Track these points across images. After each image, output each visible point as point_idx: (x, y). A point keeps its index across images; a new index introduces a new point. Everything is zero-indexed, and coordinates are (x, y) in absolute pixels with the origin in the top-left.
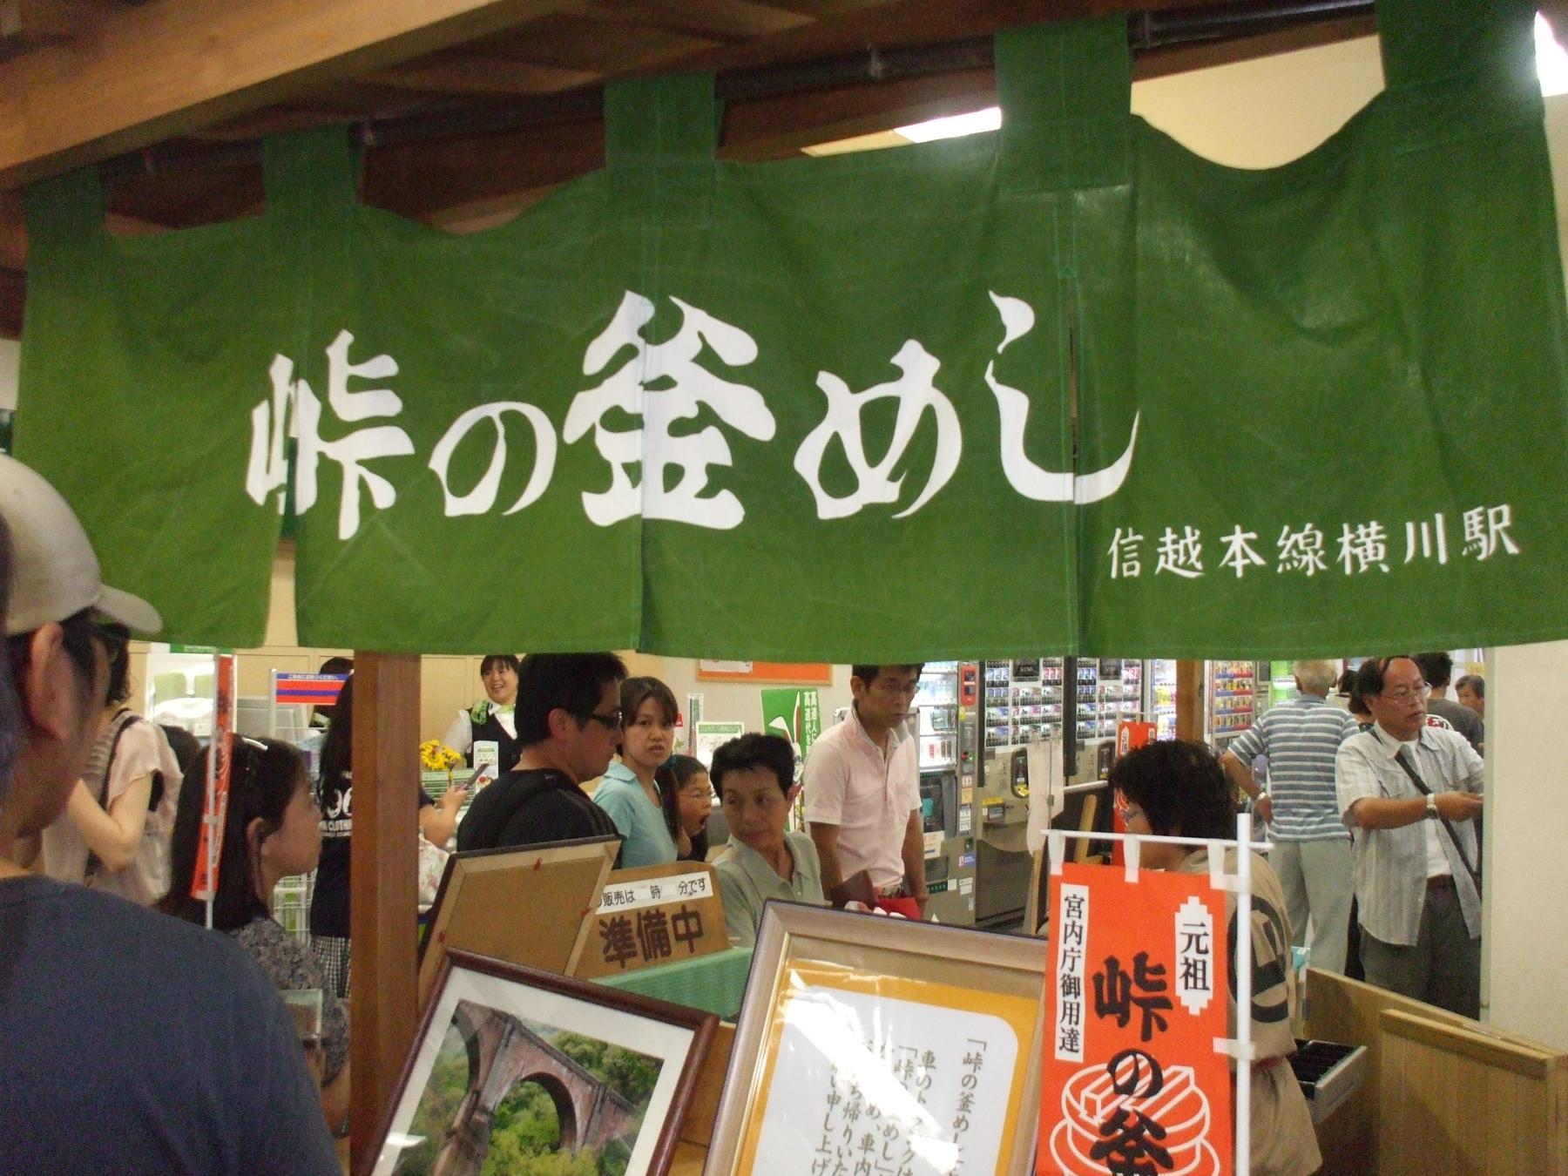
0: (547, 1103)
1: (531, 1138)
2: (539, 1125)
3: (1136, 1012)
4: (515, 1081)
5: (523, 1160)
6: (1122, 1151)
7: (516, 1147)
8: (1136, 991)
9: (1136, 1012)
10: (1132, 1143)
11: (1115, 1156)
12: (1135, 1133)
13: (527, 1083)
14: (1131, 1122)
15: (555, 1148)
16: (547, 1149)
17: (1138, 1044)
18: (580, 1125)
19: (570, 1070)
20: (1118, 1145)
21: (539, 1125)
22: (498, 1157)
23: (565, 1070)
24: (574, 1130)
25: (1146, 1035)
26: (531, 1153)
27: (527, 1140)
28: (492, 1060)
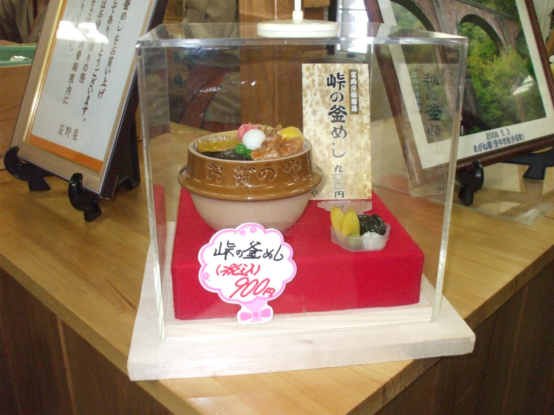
0: (479, 31)
1: (485, 54)
2: (484, 45)
3: (337, 85)
4: (457, 26)
5: (488, 67)
6: (335, 113)
7: (481, 62)
8: (337, 80)
9: (337, 85)
10: (338, 111)
11: (334, 114)
12: (339, 109)
13: (464, 24)
14: (337, 107)
15: (497, 53)
16: (495, 56)
17: (339, 91)
18: (500, 36)
19: (479, 8)
20: (334, 112)
21: (484, 45)
22: (477, 73)
23: (477, 9)
24: (500, 40)
25: (340, 89)
26: (489, 62)
27: (483, 56)
28: (436, 17)
